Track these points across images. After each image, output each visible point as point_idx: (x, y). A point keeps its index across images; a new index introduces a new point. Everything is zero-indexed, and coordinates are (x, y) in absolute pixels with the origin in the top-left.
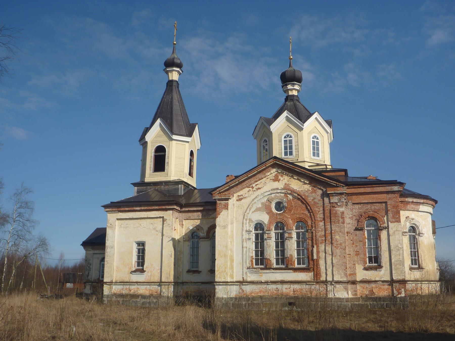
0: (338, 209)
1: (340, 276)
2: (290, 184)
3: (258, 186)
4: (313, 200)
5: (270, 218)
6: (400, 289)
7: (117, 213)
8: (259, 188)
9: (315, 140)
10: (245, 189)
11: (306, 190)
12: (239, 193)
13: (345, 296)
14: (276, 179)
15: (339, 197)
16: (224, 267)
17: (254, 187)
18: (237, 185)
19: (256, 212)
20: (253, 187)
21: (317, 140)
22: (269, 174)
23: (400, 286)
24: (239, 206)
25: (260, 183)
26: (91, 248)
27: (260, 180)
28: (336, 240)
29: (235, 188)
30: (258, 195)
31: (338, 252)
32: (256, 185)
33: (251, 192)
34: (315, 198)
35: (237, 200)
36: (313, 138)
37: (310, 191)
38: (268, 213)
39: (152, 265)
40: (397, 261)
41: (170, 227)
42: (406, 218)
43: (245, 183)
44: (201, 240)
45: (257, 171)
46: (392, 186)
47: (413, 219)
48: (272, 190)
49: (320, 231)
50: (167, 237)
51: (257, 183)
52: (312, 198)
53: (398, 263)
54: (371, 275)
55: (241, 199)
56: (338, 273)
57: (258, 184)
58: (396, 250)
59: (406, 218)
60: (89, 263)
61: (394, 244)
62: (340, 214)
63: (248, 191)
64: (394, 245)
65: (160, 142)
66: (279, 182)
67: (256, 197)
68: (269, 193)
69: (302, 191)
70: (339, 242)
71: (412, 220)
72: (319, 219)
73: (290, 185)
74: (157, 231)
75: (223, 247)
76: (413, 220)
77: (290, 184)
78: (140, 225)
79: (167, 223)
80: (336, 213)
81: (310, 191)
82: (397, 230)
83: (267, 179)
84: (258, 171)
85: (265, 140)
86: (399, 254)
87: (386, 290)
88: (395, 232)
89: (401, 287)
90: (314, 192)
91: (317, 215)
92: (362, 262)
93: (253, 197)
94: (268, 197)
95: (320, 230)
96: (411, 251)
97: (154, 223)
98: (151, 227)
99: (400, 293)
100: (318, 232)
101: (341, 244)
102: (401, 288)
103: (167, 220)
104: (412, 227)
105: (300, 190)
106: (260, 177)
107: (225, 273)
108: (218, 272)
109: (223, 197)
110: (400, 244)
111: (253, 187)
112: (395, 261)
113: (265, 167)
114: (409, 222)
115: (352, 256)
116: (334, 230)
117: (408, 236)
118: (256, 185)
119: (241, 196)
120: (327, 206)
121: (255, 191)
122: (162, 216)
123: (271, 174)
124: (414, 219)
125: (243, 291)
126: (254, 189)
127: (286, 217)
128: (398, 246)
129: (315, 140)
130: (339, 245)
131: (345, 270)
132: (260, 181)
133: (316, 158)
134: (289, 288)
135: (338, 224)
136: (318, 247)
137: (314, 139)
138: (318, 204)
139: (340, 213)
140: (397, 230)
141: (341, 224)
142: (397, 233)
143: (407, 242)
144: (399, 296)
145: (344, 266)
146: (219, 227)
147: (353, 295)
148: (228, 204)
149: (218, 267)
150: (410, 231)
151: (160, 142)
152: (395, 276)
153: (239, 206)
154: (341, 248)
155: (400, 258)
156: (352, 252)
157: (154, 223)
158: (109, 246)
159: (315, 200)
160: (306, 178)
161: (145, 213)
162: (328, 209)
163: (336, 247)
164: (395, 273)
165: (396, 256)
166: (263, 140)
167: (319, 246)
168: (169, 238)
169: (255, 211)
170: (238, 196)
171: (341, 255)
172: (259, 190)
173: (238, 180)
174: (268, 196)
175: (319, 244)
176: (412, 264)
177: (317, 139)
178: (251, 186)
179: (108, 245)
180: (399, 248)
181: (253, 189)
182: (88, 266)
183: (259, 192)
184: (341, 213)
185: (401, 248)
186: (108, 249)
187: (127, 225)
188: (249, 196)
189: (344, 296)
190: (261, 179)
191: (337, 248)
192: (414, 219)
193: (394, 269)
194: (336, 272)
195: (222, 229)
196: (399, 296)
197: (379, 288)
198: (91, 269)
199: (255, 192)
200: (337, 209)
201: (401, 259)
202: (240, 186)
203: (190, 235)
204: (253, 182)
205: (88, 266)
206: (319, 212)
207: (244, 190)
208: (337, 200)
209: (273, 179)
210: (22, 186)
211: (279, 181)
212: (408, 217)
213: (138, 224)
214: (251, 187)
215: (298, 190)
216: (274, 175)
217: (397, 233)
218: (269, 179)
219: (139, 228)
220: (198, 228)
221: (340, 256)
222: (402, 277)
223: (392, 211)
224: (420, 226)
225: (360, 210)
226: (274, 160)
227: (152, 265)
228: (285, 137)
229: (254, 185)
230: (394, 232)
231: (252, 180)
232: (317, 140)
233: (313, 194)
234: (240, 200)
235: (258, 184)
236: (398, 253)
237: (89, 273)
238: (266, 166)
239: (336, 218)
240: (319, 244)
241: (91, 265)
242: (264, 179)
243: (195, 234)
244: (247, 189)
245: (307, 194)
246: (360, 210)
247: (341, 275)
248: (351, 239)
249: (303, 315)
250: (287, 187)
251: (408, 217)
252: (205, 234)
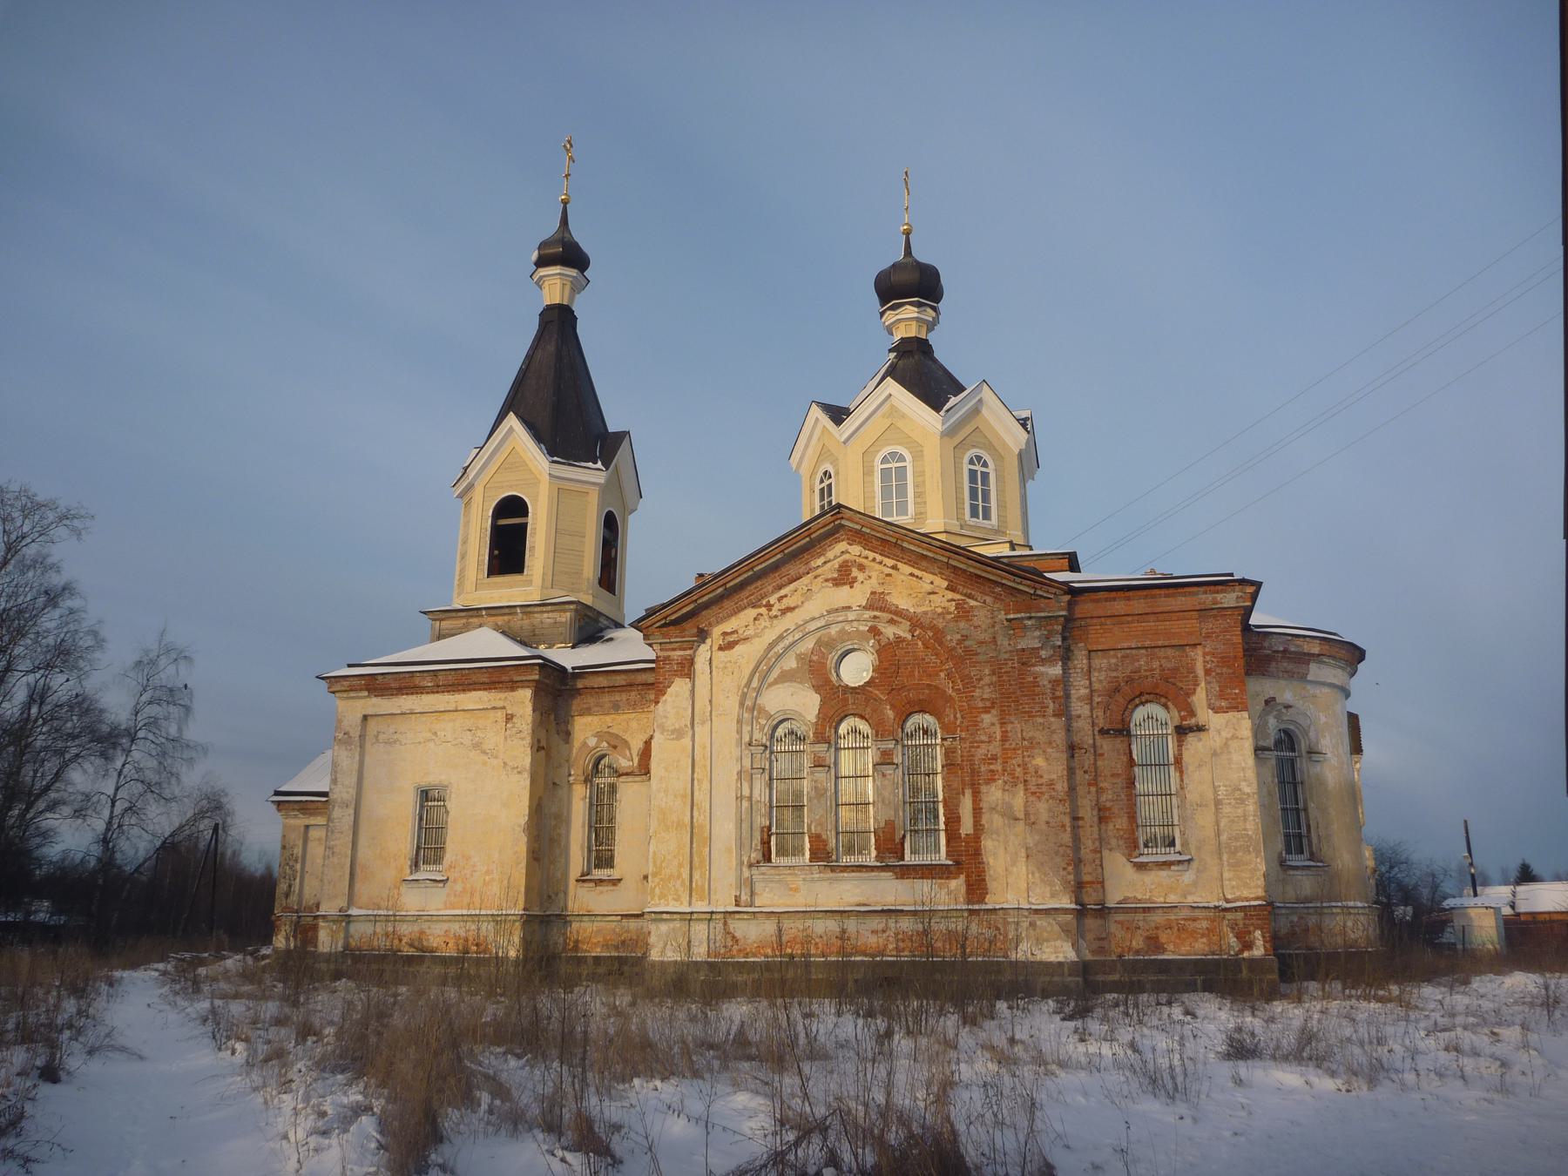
0: (1042, 669)
1: (1048, 888)
2: (889, 594)
3: (786, 603)
4: (960, 642)
5: (1480, 973)
6: (1250, 933)
7: (365, 697)
8: (790, 609)
9: (978, 468)
10: (746, 611)
11: (939, 610)
12: (728, 626)
13: (1065, 957)
14: (844, 577)
15: (1046, 633)
16: (675, 863)
17: (773, 606)
18: (721, 598)
19: (780, 686)
20: (769, 606)
21: (984, 470)
22: (820, 561)
23: (1247, 922)
24: (726, 668)
25: (792, 593)
26: (298, 810)
27: (791, 582)
28: (1036, 772)
29: (715, 609)
30: (786, 631)
31: (1041, 810)
32: (782, 597)
33: (763, 622)
34: (965, 637)
35: (721, 648)
36: (971, 462)
37: (950, 613)
38: (817, 689)
39: (468, 858)
40: (1236, 839)
41: (523, 739)
42: (1267, 702)
43: (745, 593)
44: (621, 779)
45: (783, 551)
46: (1218, 592)
47: (1288, 707)
48: (829, 612)
49: (982, 742)
50: (515, 771)
51: (783, 592)
52: (959, 637)
53: (1241, 846)
54: (1153, 887)
55: (735, 643)
56: (1042, 880)
57: (786, 596)
58: (1233, 802)
59: (1267, 702)
60: (292, 855)
61: (1227, 783)
62: (1050, 686)
63: (755, 619)
64: (1225, 786)
65: (511, 487)
66: (851, 587)
67: (781, 638)
68: (822, 622)
69: (925, 613)
70: (1046, 776)
71: (1284, 710)
72: (981, 705)
73: (887, 598)
74: (484, 752)
75: (675, 797)
76: (1290, 710)
77: (889, 594)
78: (435, 734)
79: (513, 727)
80: (1035, 684)
81: (950, 613)
82: (1234, 737)
83: (815, 577)
84: (786, 552)
85: (825, 473)
86: (1245, 816)
87: (1203, 935)
88: (1230, 742)
89: (1252, 924)
90: (963, 617)
91: (973, 691)
92: (1121, 842)
93: (770, 636)
94: (818, 635)
95: (984, 738)
96: (1283, 809)
97: (477, 728)
98: (467, 738)
99: (1248, 946)
100: (978, 747)
101: (1052, 784)
102: (1252, 928)
103: (515, 720)
104: (1286, 732)
105: (920, 610)
106: (793, 573)
107: (679, 882)
108: (657, 880)
109: (676, 637)
110: (1245, 780)
111: (769, 606)
112: (1230, 839)
113: (808, 539)
114: (1275, 717)
115: (1088, 825)
116: (1030, 738)
117: (1273, 762)
118: (782, 597)
119: (732, 633)
120: (1005, 660)
121: (776, 617)
122: (500, 704)
123: (825, 563)
124: (1291, 707)
125: (737, 941)
126: (774, 612)
127: (875, 700)
128: (1240, 790)
129: (978, 468)
130: (1044, 789)
131: (1064, 869)
132: (792, 586)
133: (980, 521)
134: (884, 931)
135: (1040, 720)
136: (976, 795)
137: (974, 464)
138: (977, 654)
139: (1046, 683)
140: (1234, 737)
141: (1053, 719)
142: (1234, 744)
143: (1270, 779)
144: (1246, 954)
145: (1063, 856)
146: (662, 733)
147: (1093, 952)
148: (691, 662)
149: (658, 862)
150: (1278, 744)
151: (511, 487)
152: (1233, 887)
153: (726, 668)
154: (1052, 797)
155: (1245, 830)
156: (1089, 809)
157: (477, 728)
158: (339, 800)
159: (967, 643)
160: (940, 573)
161: (451, 697)
162: (1009, 670)
163: (1035, 793)
164: (1229, 880)
165: (1233, 821)
166: (820, 474)
167: (979, 792)
168: (519, 773)
169: (776, 682)
170: (725, 634)
171: (1051, 820)
172: (789, 614)
173: (721, 583)
174: (818, 635)
175: (979, 784)
176: (1289, 851)
177: (985, 465)
178: (764, 602)
179: (335, 796)
180: (1244, 794)
181: (770, 610)
182: (288, 864)
183: (789, 621)
184: (1050, 682)
185: (1248, 794)
186: (336, 808)
187: (395, 737)
188: (757, 635)
189: (1061, 955)
190: (795, 580)
191: (1039, 797)
192: (1291, 707)
193: (1228, 865)
194: (1037, 875)
195: (673, 739)
196: (1246, 954)
197: (1178, 930)
198: (298, 875)
199: (775, 621)
200: (1037, 669)
201: (1250, 833)
202: (728, 604)
203: (588, 765)
204: (770, 588)
205: (288, 864)
206: (980, 679)
207: (742, 615)
208: (1037, 641)
209: (834, 579)
210: (160, 642)
211: (852, 584)
212: (1273, 699)
213: (430, 731)
214: (765, 606)
215: (912, 610)
216: (837, 566)
217: (1234, 744)
218: (820, 579)
219: (431, 745)
220: (612, 743)
221: (1047, 823)
222: (1254, 890)
223: (1218, 674)
224: (1312, 728)
225: (1115, 674)
226: (835, 517)
227: (468, 858)
228: (884, 460)
229: (773, 599)
230: (1226, 744)
231: (768, 584)
232: (984, 470)
233: (962, 624)
234: (730, 646)
235: (786, 596)
236: (1240, 811)
237: (290, 886)
238: (812, 536)
239: (1034, 699)
240: (979, 784)
241: (300, 861)
242: (805, 580)
243: (605, 761)
244: (751, 613)
245: (940, 624)
246: (1115, 674)
247: (1052, 885)
248: (1086, 768)
249: (756, 1029)
250: (877, 602)
251: (1273, 699)
252: (636, 760)
